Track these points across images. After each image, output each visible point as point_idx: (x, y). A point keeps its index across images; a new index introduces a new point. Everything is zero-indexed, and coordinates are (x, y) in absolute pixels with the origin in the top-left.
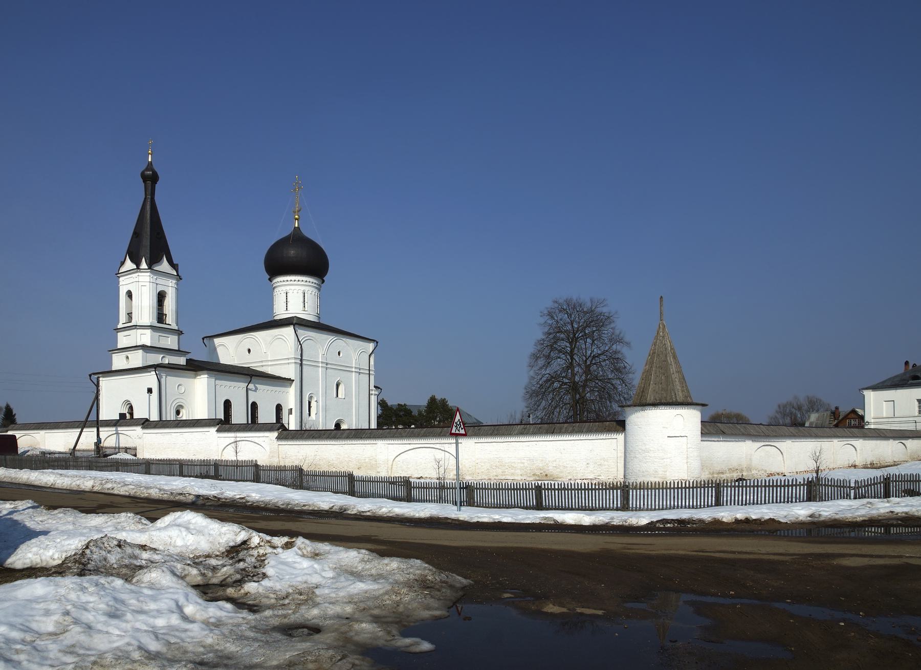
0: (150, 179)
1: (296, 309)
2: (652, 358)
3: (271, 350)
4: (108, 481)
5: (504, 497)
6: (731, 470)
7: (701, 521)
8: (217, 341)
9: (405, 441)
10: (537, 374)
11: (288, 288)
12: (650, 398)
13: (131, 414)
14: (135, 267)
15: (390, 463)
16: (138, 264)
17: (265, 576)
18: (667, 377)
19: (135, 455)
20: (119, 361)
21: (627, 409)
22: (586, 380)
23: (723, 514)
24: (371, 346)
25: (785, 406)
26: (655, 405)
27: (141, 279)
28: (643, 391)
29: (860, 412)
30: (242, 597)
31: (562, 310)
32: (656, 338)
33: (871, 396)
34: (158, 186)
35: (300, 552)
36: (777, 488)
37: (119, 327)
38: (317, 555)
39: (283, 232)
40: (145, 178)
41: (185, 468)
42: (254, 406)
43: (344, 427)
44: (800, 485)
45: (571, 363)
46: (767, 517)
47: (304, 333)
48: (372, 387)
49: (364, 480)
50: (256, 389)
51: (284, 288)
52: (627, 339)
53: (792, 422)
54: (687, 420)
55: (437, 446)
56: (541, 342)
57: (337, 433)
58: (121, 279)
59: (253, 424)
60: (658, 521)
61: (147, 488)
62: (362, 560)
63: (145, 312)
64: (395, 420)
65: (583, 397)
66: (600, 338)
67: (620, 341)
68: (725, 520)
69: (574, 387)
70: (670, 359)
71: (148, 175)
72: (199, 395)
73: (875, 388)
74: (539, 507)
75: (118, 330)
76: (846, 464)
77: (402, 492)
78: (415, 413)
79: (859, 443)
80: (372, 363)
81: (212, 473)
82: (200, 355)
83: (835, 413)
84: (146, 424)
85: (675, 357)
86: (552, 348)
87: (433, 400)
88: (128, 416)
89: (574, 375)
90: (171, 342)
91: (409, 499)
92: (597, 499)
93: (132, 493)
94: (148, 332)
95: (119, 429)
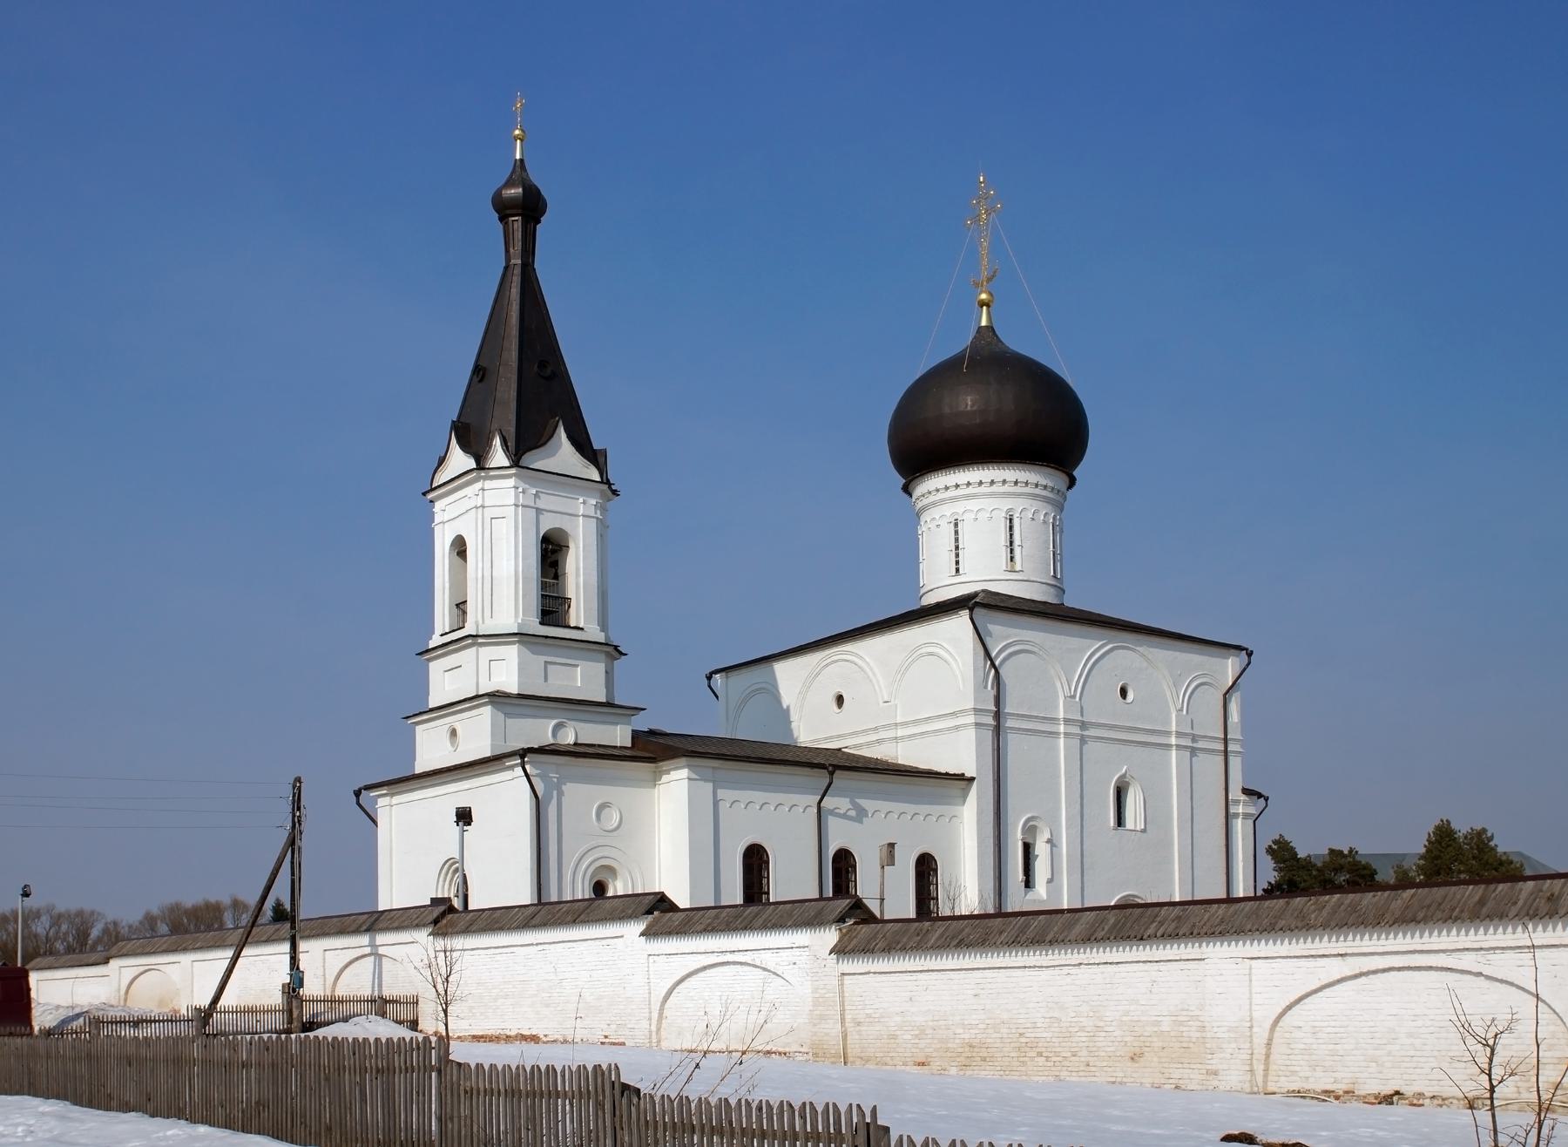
0: (524, 209)
1: (985, 570)
3: (900, 695)
11: (959, 507)
14: (472, 464)
15: (1261, 1034)
19: (414, 1025)
24: (1230, 666)
37: (432, 644)
39: (961, 342)
40: (503, 209)
43: (617, 888)
47: (1005, 633)
48: (1236, 793)
50: (861, 814)
51: (948, 510)
55: (1467, 961)
58: (438, 506)
59: (754, 901)
63: (501, 589)
64: (1312, 888)
71: (512, 199)
72: (665, 830)
87: (1443, 836)
90: (582, 678)
94: (511, 652)
95: (381, 939)
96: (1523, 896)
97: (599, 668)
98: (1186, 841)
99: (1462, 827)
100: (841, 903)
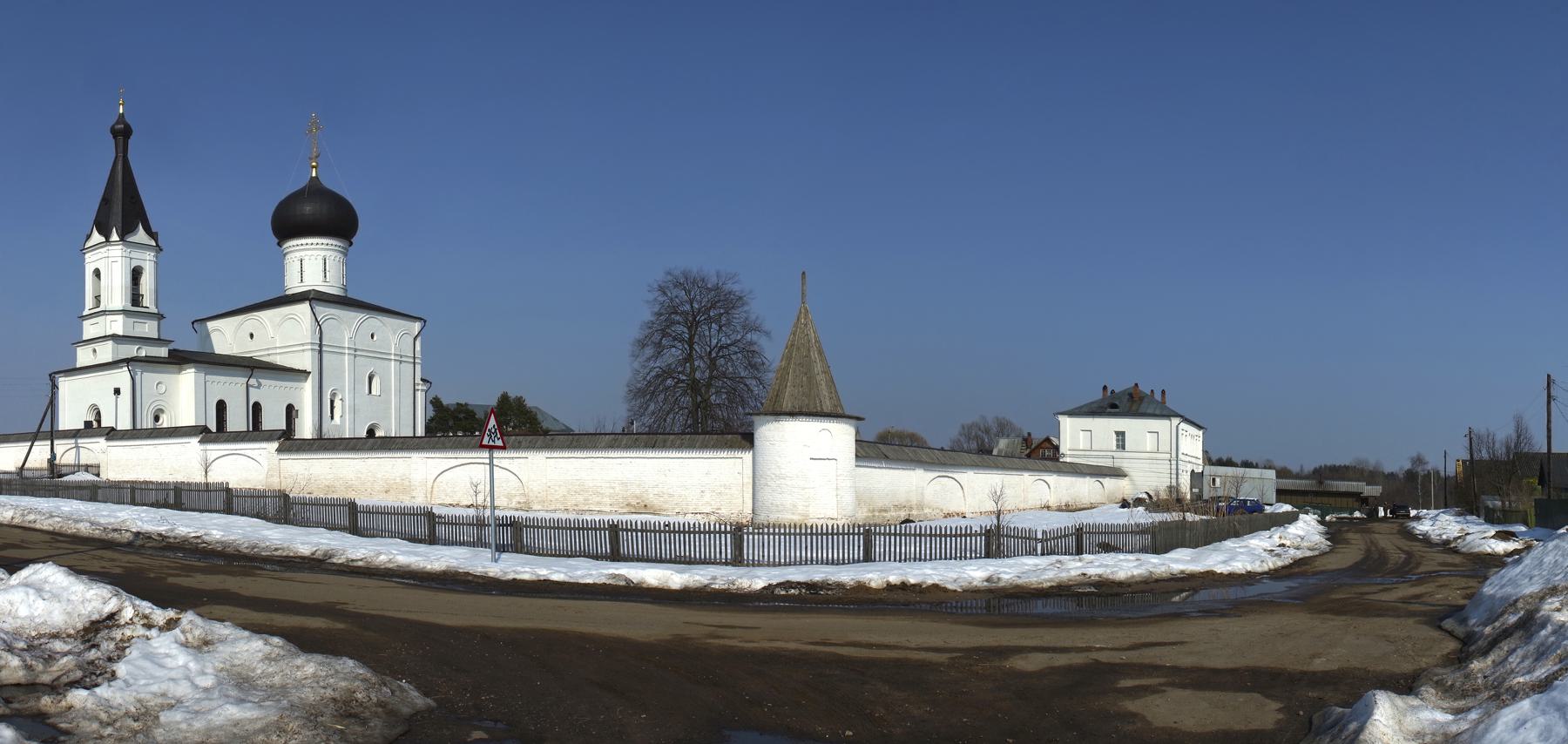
0: (122, 133)
1: (314, 279)
2: (790, 353)
4: (31, 511)
5: (565, 541)
6: (898, 507)
7: (840, 586)
8: (211, 325)
9: (450, 455)
10: (644, 367)
12: (787, 405)
13: (99, 422)
15: (430, 484)
16: (107, 237)
17: (113, 676)
20: (84, 357)
21: (756, 419)
22: (711, 378)
24: (417, 326)
25: (970, 427)
26: (793, 414)
27: (111, 253)
28: (778, 395)
29: (1055, 441)
30: (60, 714)
31: (677, 285)
32: (796, 326)
33: (1067, 423)
35: (183, 638)
36: (949, 540)
38: (206, 643)
39: (302, 183)
40: (115, 133)
41: (138, 493)
42: (257, 408)
43: (379, 433)
44: (976, 535)
45: (690, 355)
46: (930, 582)
47: (323, 311)
48: (418, 380)
49: (371, 512)
52: (767, 326)
53: (977, 448)
54: (839, 437)
56: (650, 325)
57: (372, 442)
59: (256, 432)
60: (779, 585)
61: (76, 521)
62: (268, 658)
63: (115, 293)
64: (450, 426)
65: (704, 399)
66: (729, 323)
67: (756, 329)
68: (873, 585)
69: (694, 387)
70: (815, 355)
72: (184, 394)
73: (1072, 413)
74: (615, 556)
76: (1038, 504)
77: (423, 530)
79: (1052, 479)
80: (418, 348)
81: (172, 501)
82: (188, 344)
83: (1027, 440)
84: (112, 434)
85: (820, 352)
87: (504, 398)
88: (95, 424)
89: (693, 370)
90: (149, 329)
91: (432, 540)
92: (697, 547)
93: (57, 527)
94: (120, 318)
96: (1197, 518)
99: (512, 394)
100: (287, 440)
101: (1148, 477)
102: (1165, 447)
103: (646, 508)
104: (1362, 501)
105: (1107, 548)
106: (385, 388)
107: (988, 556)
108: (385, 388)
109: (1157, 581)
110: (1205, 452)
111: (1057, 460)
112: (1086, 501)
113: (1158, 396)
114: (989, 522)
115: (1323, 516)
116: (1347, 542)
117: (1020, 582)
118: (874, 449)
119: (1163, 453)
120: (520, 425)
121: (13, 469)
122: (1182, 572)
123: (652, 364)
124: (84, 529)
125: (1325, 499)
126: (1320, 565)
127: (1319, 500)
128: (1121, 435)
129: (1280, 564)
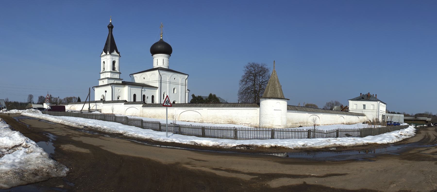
0: (111, 27)
3: (151, 78)
4: (65, 120)
7: (257, 146)
8: (134, 75)
12: (268, 96)
16: (106, 53)
18: (275, 89)
22: (260, 90)
23: (266, 143)
24: (186, 76)
25: (329, 103)
26: (270, 98)
31: (251, 66)
33: (351, 102)
34: (113, 29)
39: (158, 40)
40: (109, 27)
42: (144, 96)
44: (305, 132)
45: (254, 84)
47: (162, 72)
48: (186, 90)
53: (329, 109)
54: (283, 104)
56: (244, 76)
57: (168, 104)
59: (135, 102)
60: (237, 146)
63: (109, 68)
64: (197, 101)
68: (267, 146)
69: (255, 92)
70: (276, 83)
72: (125, 93)
73: (352, 100)
75: (100, 73)
76: (341, 123)
77: (158, 127)
78: (204, 99)
79: (345, 116)
80: (187, 82)
82: (128, 80)
83: (342, 106)
86: (248, 78)
87: (211, 95)
90: (117, 76)
94: (109, 73)
97: (119, 75)
98: (181, 96)
99: (213, 94)
100: (144, 103)
101: (370, 116)
102: (376, 108)
103: (232, 123)
104: (426, 122)
105: (348, 136)
106: (177, 92)
107: (308, 137)
108: (177, 92)
109: (358, 146)
110: (386, 110)
111: (348, 111)
112: (354, 122)
113: (375, 96)
114: (312, 128)
115: (416, 126)
116: (420, 133)
117: (312, 146)
118: (291, 108)
119: (375, 110)
120: (212, 101)
121: (79, 110)
122: (368, 143)
123: (244, 86)
124: (74, 125)
125: (417, 122)
126: (410, 141)
127: (415, 122)
128: (364, 105)
129: (398, 140)
